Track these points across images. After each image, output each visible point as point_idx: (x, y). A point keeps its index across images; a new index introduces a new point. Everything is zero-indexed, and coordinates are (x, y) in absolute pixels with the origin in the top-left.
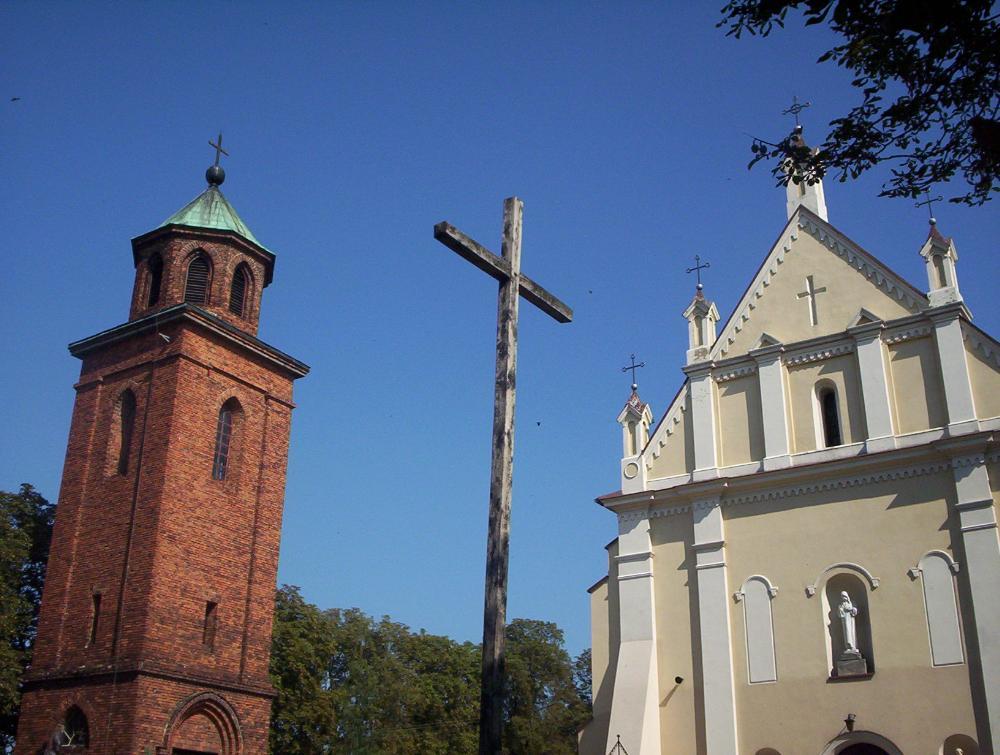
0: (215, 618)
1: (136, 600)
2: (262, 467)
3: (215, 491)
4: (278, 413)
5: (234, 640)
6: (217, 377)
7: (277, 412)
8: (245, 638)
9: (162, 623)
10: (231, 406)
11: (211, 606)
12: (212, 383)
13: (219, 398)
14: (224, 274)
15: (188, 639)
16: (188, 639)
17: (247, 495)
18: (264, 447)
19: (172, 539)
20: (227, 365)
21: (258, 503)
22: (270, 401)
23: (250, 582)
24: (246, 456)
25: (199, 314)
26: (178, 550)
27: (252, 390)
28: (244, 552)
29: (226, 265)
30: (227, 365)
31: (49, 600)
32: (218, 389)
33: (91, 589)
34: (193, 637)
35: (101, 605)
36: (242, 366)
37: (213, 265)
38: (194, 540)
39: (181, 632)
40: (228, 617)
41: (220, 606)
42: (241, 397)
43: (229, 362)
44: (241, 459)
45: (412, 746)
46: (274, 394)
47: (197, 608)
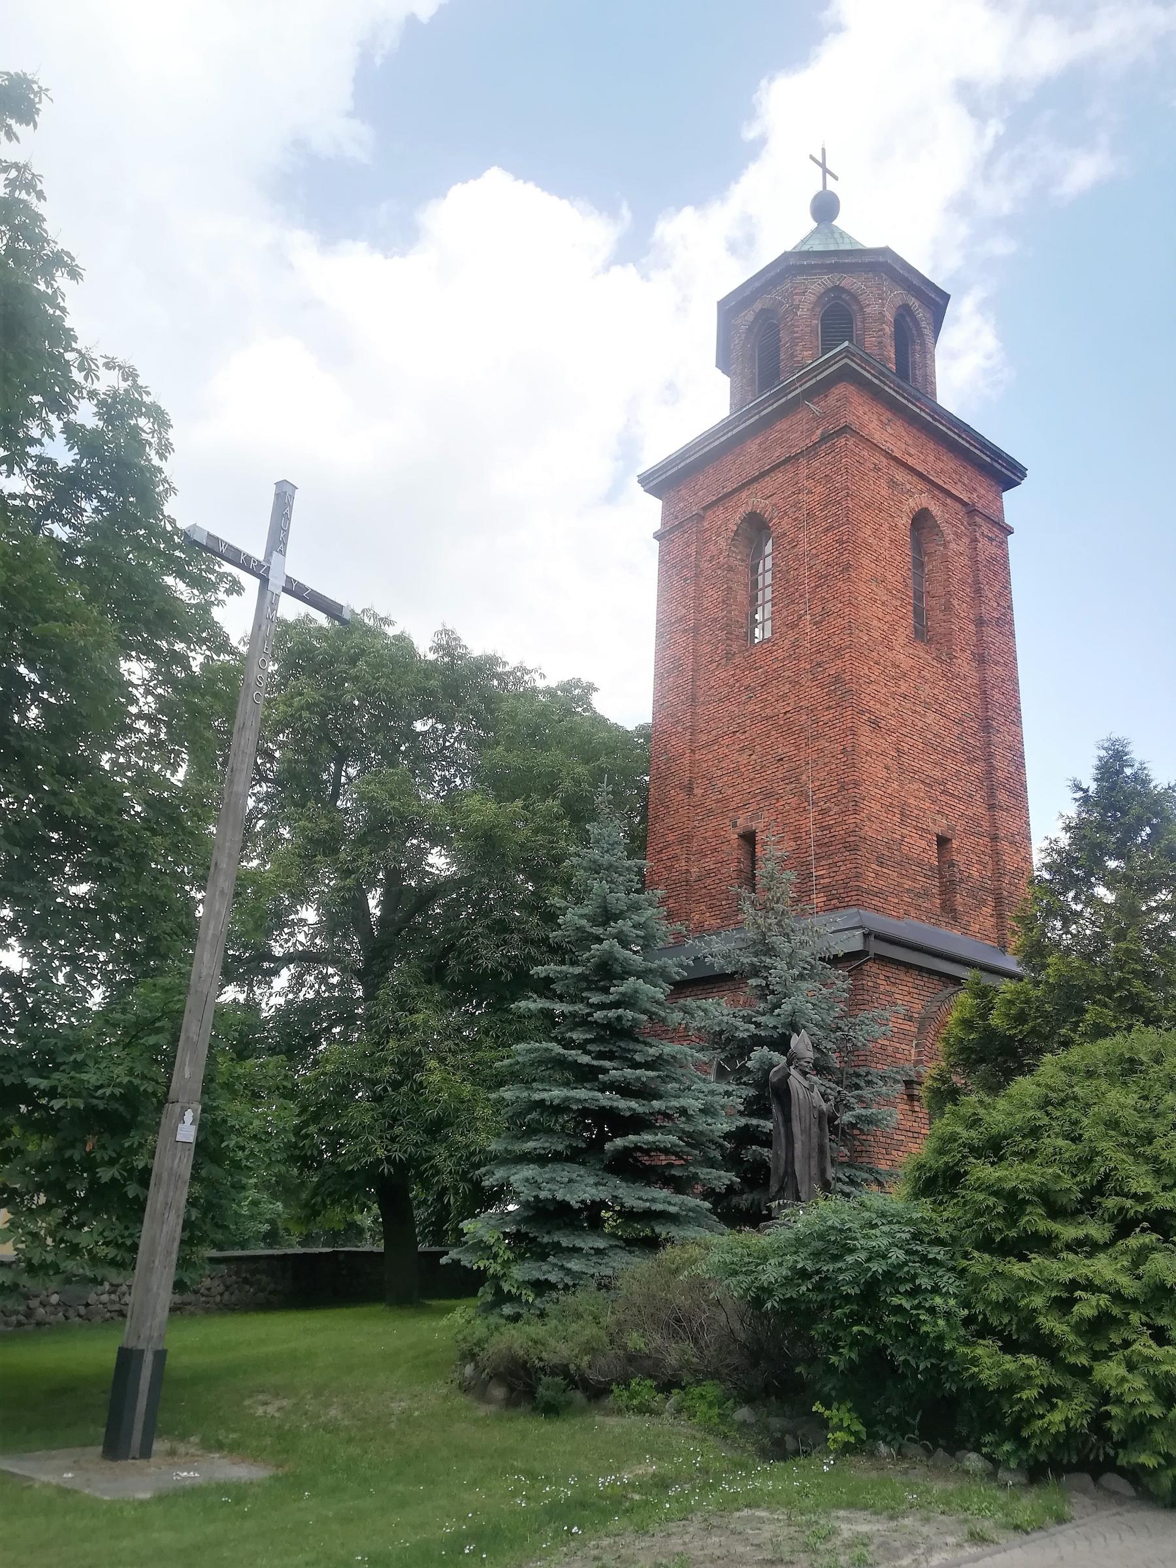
0: (952, 864)
1: (829, 828)
2: (980, 622)
3: (922, 654)
4: (991, 539)
5: (984, 902)
6: (901, 476)
7: (987, 536)
8: (999, 901)
9: (881, 864)
10: (921, 519)
11: (943, 842)
12: (892, 483)
13: (905, 508)
14: (881, 318)
15: (918, 895)
16: (918, 895)
17: (964, 664)
18: (978, 591)
19: (875, 724)
20: (911, 455)
21: (983, 680)
22: (978, 520)
23: (991, 807)
24: (955, 602)
25: (869, 364)
26: (885, 743)
27: (949, 501)
28: (976, 759)
29: (883, 305)
30: (911, 455)
31: (660, 852)
32: (903, 493)
33: (735, 825)
34: (925, 894)
35: (758, 848)
36: (931, 458)
37: (862, 308)
38: (904, 731)
39: (908, 884)
40: (969, 863)
41: (955, 843)
42: (935, 509)
43: (912, 451)
44: (948, 608)
45: (595, 1330)
46: (979, 506)
47: (923, 844)
